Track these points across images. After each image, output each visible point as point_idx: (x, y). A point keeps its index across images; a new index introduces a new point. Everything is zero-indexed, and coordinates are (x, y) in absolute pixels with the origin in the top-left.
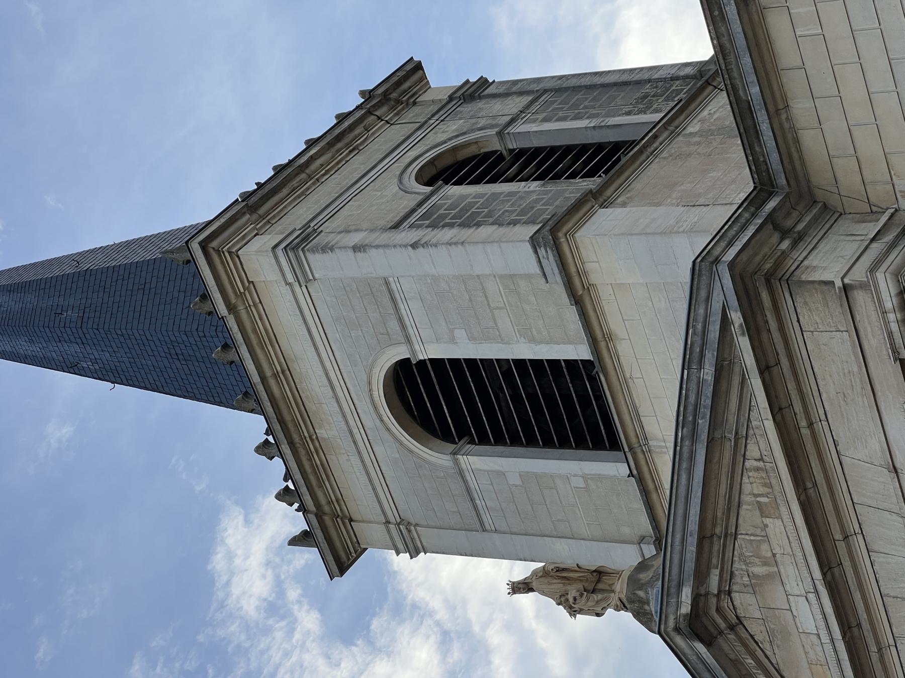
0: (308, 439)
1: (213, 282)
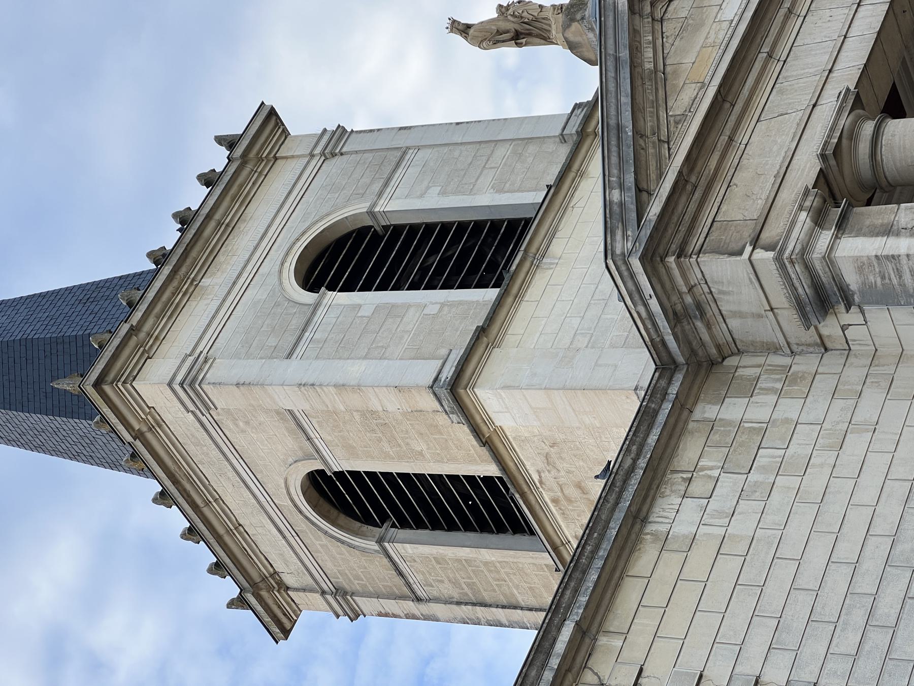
0: (189, 281)
1: (253, 132)
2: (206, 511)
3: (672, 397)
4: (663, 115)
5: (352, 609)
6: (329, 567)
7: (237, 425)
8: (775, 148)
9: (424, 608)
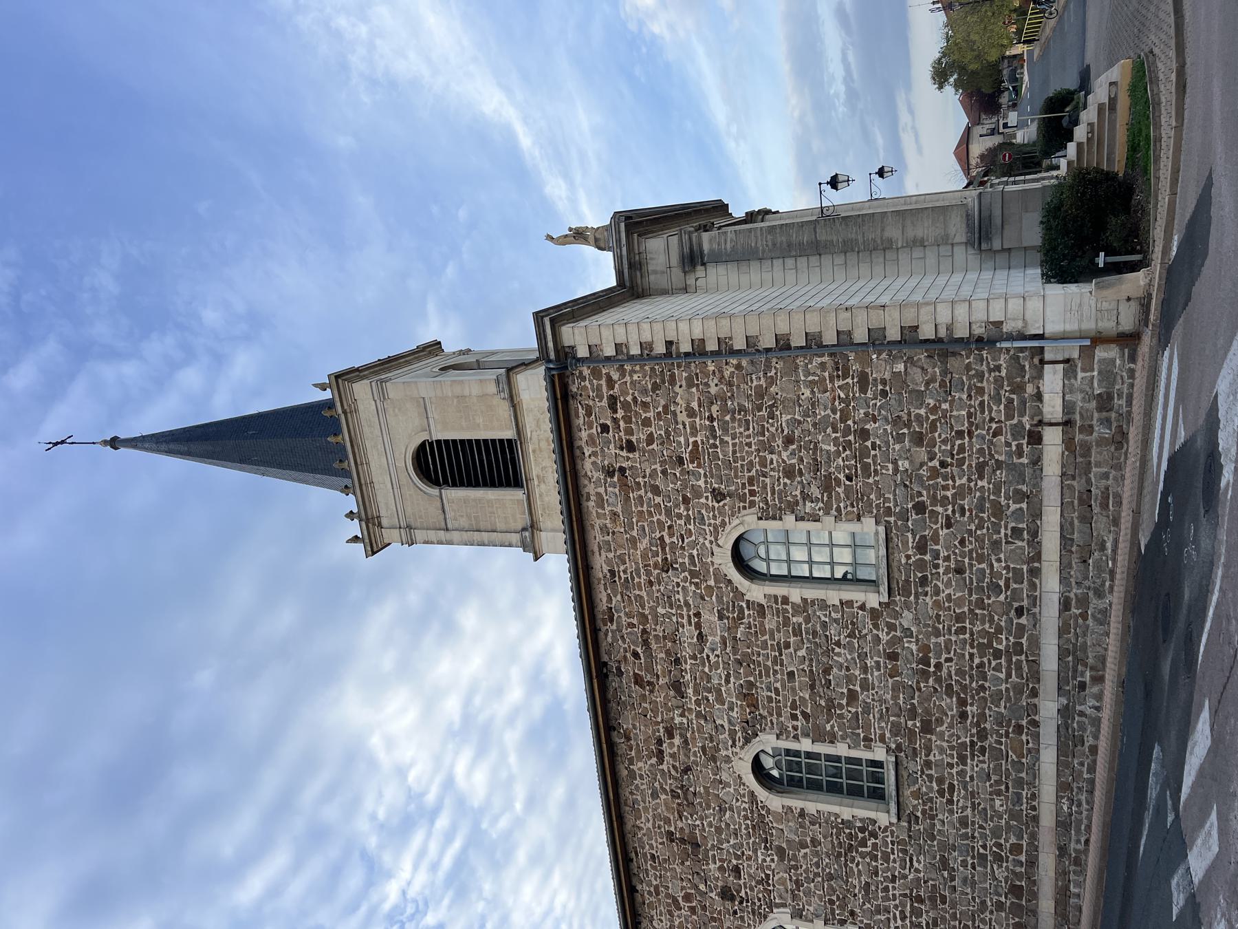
2: (360, 467)
5: (412, 539)
6: (409, 510)
7: (394, 411)
9: (448, 536)
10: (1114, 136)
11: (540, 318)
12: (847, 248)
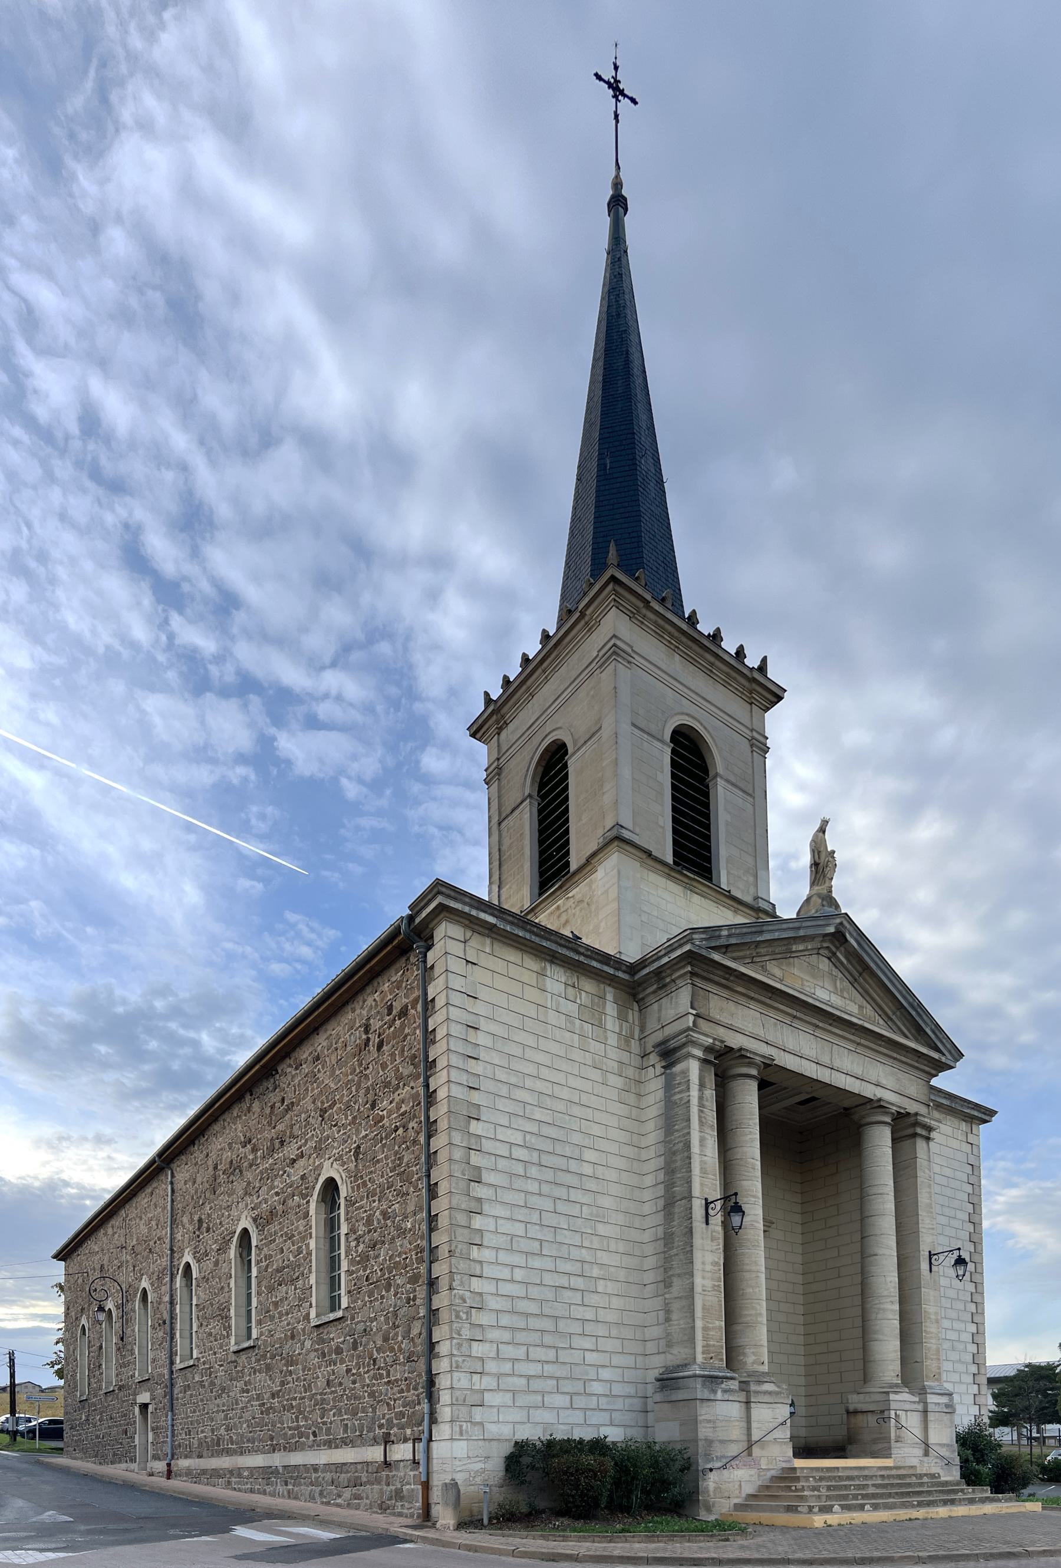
2: (540, 671)
3: (617, 974)
4: (767, 958)
8: (746, 1023)
10: (764, 1511)
11: (435, 890)
12: (668, 1239)
